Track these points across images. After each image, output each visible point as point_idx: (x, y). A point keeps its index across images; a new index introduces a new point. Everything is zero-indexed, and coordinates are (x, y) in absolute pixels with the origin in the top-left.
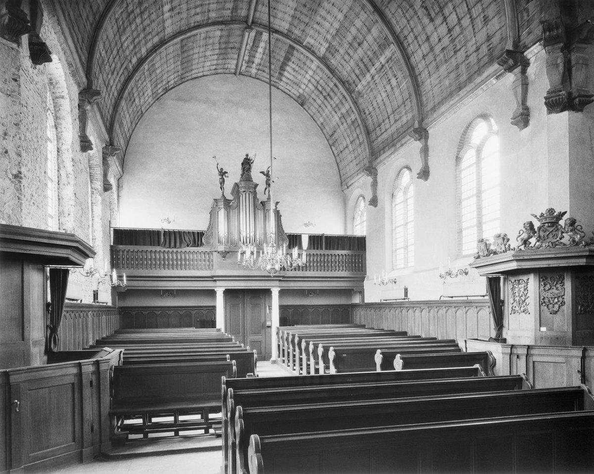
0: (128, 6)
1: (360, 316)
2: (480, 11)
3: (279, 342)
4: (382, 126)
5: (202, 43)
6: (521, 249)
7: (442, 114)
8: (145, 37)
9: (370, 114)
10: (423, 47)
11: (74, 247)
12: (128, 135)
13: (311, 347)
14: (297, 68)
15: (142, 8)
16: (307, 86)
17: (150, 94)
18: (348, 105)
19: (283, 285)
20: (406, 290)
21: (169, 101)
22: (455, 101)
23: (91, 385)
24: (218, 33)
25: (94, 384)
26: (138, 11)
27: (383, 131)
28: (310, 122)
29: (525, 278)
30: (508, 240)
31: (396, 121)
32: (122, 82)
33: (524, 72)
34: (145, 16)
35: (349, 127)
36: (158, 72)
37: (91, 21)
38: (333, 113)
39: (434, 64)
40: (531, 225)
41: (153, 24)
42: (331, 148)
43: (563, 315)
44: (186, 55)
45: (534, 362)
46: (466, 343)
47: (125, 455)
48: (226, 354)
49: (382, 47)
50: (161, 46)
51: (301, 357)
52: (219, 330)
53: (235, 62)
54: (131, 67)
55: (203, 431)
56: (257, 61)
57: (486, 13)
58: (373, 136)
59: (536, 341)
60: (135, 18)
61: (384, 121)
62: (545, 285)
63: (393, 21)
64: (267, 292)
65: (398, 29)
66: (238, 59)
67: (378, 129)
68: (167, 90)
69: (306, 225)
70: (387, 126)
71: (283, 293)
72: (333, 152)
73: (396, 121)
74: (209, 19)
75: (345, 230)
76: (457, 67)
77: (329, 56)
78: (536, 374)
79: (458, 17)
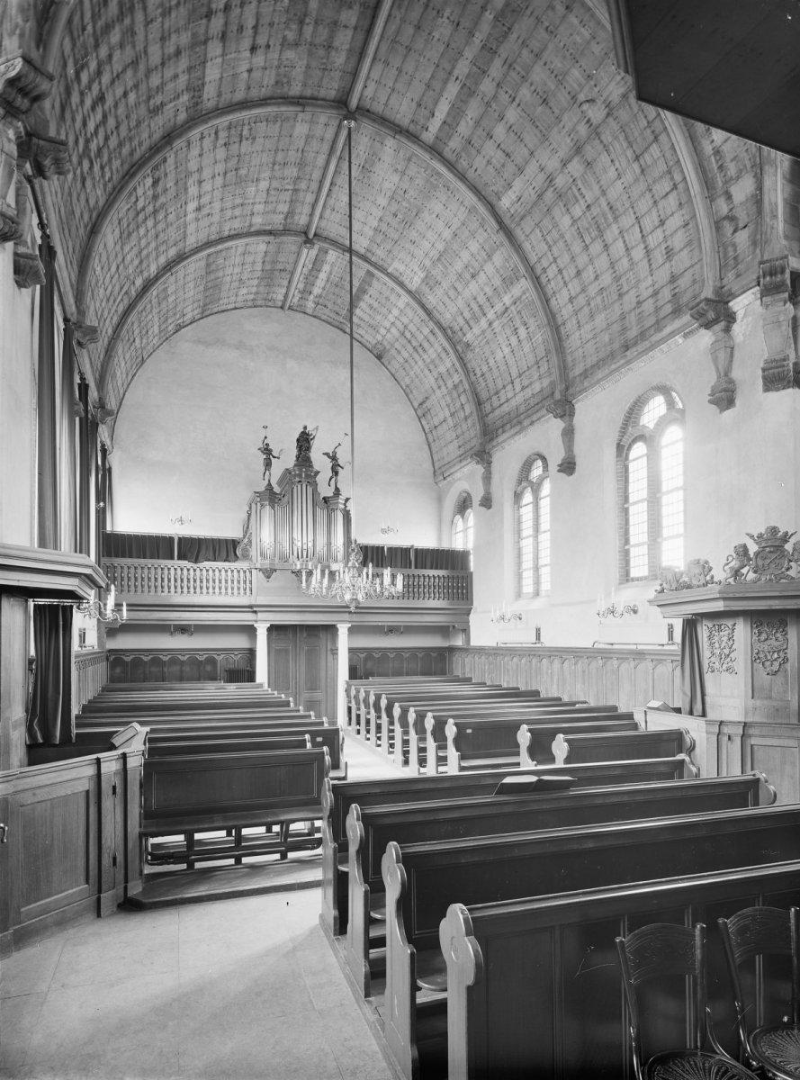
0: (137, 200)
1: (461, 666)
2: (661, 238)
3: (350, 702)
4: (502, 393)
5: (238, 260)
6: (730, 583)
7: (598, 381)
8: (156, 248)
9: (482, 375)
10: (570, 285)
11: (85, 575)
12: (122, 392)
13: (412, 717)
14: (376, 305)
15: (158, 204)
16: (388, 331)
17: (156, 331)
18: (450, 361)
19: (355, 620)
20: (538, 631)
21: (185, 343)
22: (618, 364)
23: (114, 792)
24: (263, 247)
25: (119, 790)
26: (150, 208)
27: (502, 401)
28: (390, 383)
29: (730, 623)
30: (710, 569)
31: (523, 388)
32: (119, 313)
33: (727, 330)
34: (161, 216)
35: (450, 393)
36: (170, 300)
37: (86, 221)
38: (427, 371)
39: (586, 310)
40: (745, 548)
41: (170, 228)
42: (420, 422)
43: (786, 676)
44: (212, 276)
45: (752, 746)
46: (646, 714)
47: (168, 901)
48: (304, 733)
49: (509, 282)
50: (179, 263)
51: (379, 722)
52: (261, 685)
53: (284, 291)
54: (133, 293)
55: (277, 856)
56: (317, 291)
57: (669, 243)
58: (488, 407)
59: (746, 713)
60: (146, 219)
61: (504, 387)
62: (760, 633)
63: (527, 246)
64: (331, 629)
65: (533, 258)
66: (288, 288)
67: (494, 398)
68: (179, 328)
69: (384, 531)
70: (510, 395)
71: (352, 631)
72: (423, 428)
73: (523, 388)
74: (251, 225)
75: (440, 539)
76: (623, 317)
77: (426, 289)
78: (755, 762)
79: (626, 246)
